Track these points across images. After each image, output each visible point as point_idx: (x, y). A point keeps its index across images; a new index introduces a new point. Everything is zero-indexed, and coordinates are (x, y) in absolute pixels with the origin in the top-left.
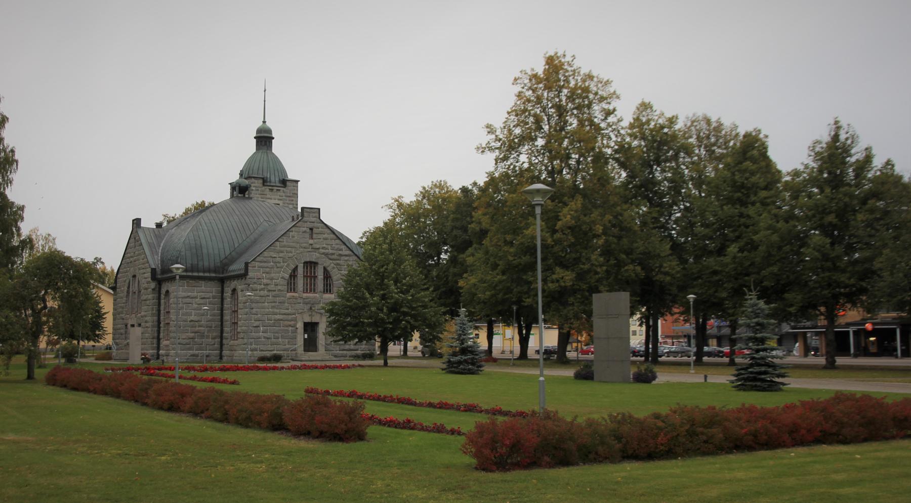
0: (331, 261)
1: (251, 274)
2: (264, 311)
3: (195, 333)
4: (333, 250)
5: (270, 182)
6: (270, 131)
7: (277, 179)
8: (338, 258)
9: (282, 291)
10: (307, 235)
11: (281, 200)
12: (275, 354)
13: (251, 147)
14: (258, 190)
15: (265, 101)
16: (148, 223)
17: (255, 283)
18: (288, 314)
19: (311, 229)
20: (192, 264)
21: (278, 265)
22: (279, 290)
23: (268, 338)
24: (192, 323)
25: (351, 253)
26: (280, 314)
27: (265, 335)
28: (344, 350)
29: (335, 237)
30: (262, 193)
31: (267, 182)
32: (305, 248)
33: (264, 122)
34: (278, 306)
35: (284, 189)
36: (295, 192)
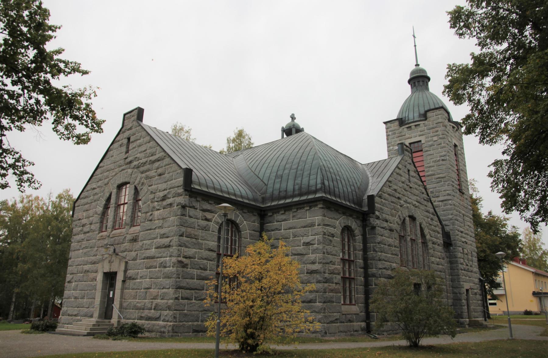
2: (386, 256)
6: (424, 71)
9: (89, 240)
11: (423, 135)
12: (134, 325)
14: (395, 134)
15: (415, 46)
30: (400, 135)
33: (417, 65)
35: (426, 122)
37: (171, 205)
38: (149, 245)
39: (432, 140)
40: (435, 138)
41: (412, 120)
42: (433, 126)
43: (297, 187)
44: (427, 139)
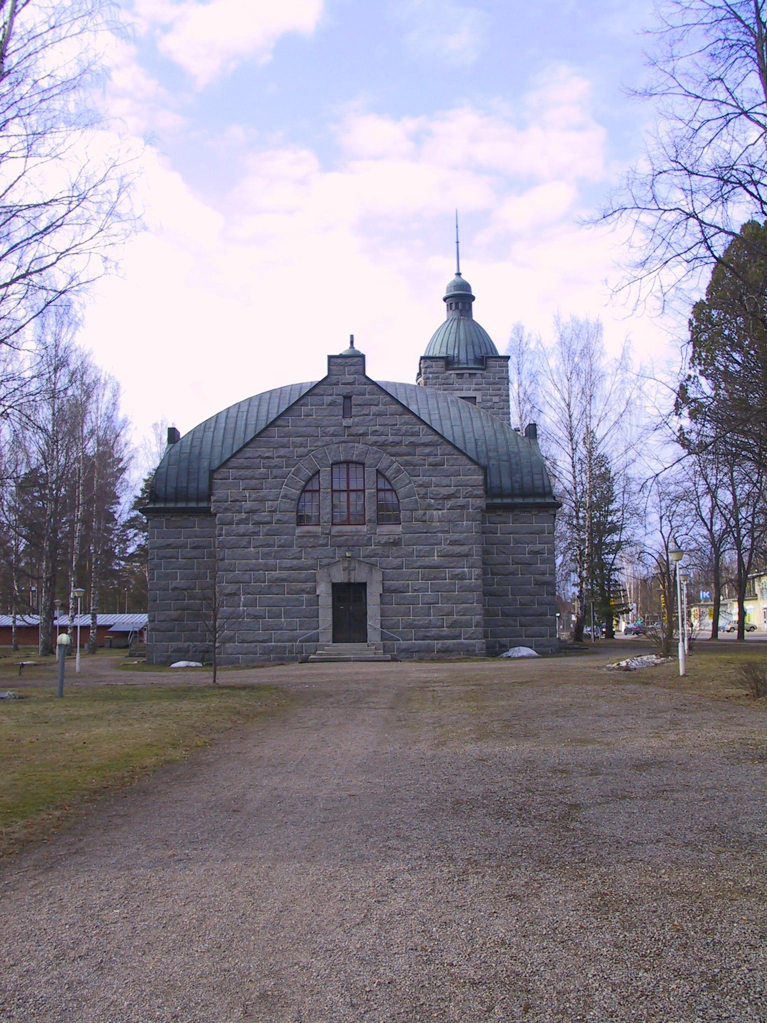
0: (393, 458)
1: (218, 493)
3: (183, 610)
4: (396, 435)
5: (459, 362)
7: (471, 357)
8: (409, 449)
10: (339, 410)
13: (440, 314)
14: (437, 378)
15: (458, 242)
16: (183, 431)
17: (227, 510)
18: (300, 569)
19: (347, 397)
20: (176, 488)
21: (276, 472)
22: (279, 521)
23: (255, 617)
24: (176, 593)
25: (436, 438)
26: (281, 569)
27: (251, 610)
28: (425, 638)
29: (400, 409)
31: (454, 364)
32: (333, 435)
33: (459, 274)
34: (276, 552)
35: (485, 373)
36: (504, 375)
37: (463, 507)
38: (427, 552)
39: (491, 400)
40: (496, 399)
41: (464, 364)
42: (494, 381)
43: (516, 485)
44: (484, 397)
